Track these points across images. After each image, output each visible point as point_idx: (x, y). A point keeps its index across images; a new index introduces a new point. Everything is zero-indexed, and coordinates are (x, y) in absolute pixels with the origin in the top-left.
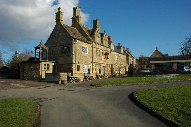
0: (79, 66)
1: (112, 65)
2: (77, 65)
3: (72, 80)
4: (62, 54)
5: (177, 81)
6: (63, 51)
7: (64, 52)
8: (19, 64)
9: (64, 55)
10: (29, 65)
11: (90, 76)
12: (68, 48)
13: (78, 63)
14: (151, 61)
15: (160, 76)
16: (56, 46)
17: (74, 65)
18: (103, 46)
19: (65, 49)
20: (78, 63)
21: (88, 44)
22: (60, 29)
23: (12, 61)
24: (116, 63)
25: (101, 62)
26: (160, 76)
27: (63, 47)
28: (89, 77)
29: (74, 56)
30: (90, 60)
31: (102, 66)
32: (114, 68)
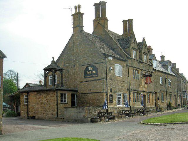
0: (111, 96)
4: (85, 78)
5: (160, 124)
6: (88, 73)
7: (88, 75)
9: (88, 79)
10: (36, 95)
16: (74, 66)
17: (105, 94)
19: (91, 70)
20: (111, 91)
29: (106, 80)
31: (142, 96)
32: (158, 99)
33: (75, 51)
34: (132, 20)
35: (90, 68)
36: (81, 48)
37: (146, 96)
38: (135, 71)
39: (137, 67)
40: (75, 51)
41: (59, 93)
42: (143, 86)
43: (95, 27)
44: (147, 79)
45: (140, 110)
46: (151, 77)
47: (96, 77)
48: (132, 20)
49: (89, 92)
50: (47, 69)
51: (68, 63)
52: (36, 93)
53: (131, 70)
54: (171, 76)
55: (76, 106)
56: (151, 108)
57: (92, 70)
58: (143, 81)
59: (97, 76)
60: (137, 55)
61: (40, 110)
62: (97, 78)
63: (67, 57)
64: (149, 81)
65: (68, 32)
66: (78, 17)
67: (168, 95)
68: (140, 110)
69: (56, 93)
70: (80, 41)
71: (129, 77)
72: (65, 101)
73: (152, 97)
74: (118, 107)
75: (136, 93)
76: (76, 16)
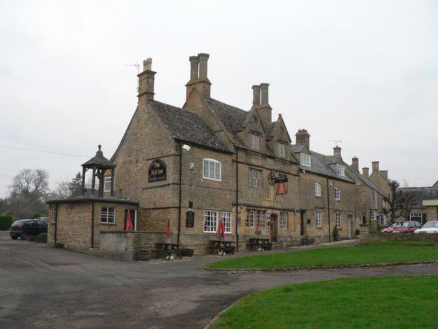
1: (302, 212)
3: (259, 245)
6: (153, 173)
8: (81, 177)
10: (67, 208)
11: (262, 240)
13: (191, 205)
14: (427, 198)
18: (272, 158)
19: (157, 168)
20: (191, 205)
21: (222, 155)
23: (25, 192)
24: (316, 205)
25: (266, 204)
28: (222, 245)
30: (228, 196)
32: (309, 221)
34: (268, 85)
36: (147, 130)
37: (279, 218)
39: (260, 164)
41: (98, 208)
42: (270, 199)
43: (189, 96)
44: (279, 186)
48: (268, 85)
49: (152, 206)
50: (88, 165)
51: (130, 156)
53: (243, 169)
54: (340, 183)
55: (135, 230)
56: (290, 237)
58: (272, 190)
59: (165, 179)
61: (70, 233)
65: (129, 104)
66: (147, 77)
67: (333, 216)
69: (91, 207)
71: (237, 181)
72: (111, 220)
73: (294, 219)
74: (207, 236)
75: (255, 210)
76: (143, 77)
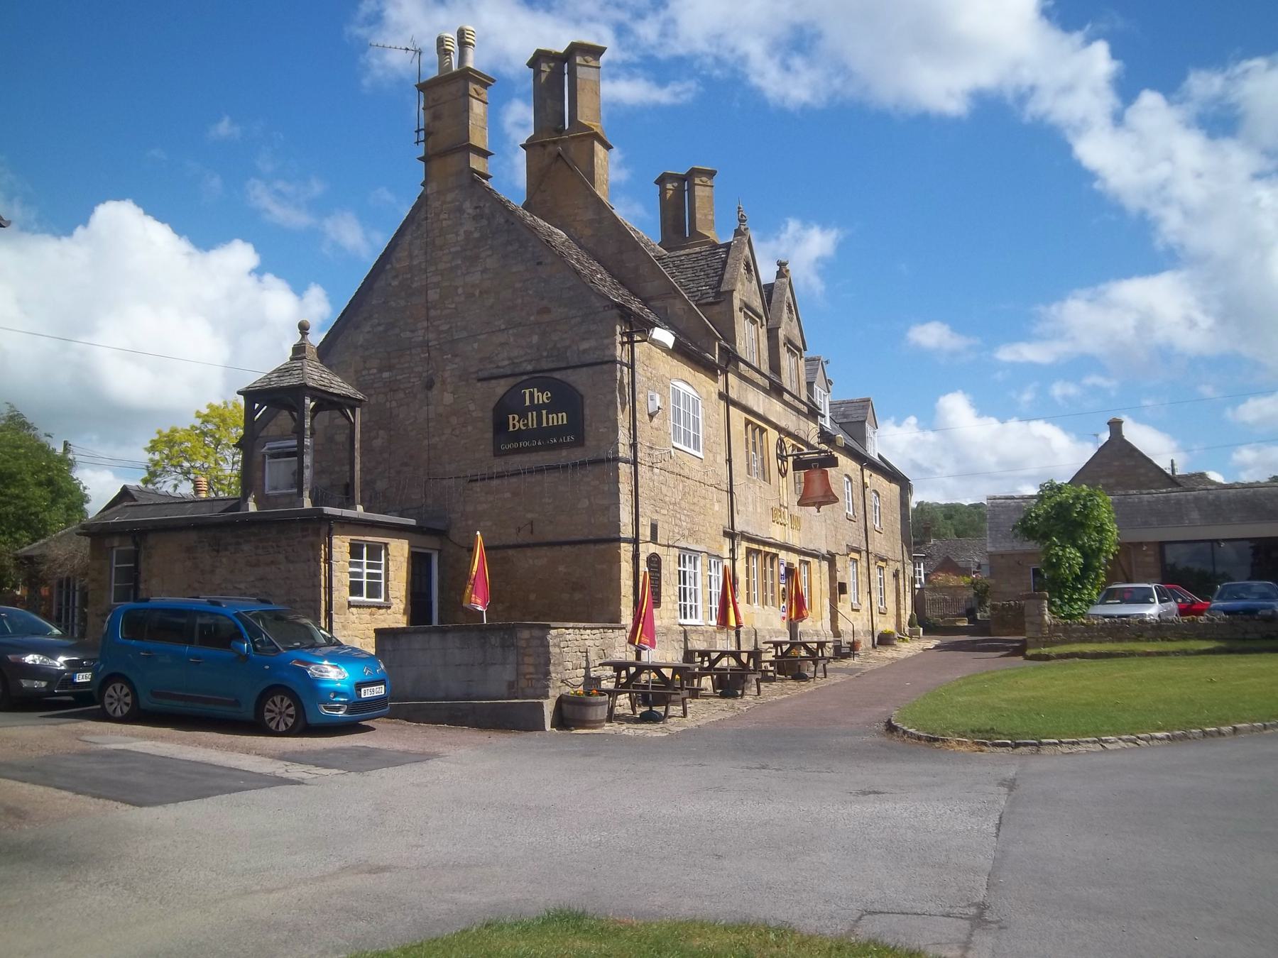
0: (654, 561)
2: (646, 550)
4: (498, 453)
6: (515, 423)
7: (518, 436)
9: (518, 461)
12: (566, 399)
15: (903, 551)
16: (429, 385)
17: (626, 550)
19: (538, 408)
22: (468, 225)
26: (903, 551)
27: (515, 392)
33: (433, 295)
35: (532, 395)
36: (476, 278)
38: (754, 431)
40: (433, 295)
45: (719, 659)
46: (831, 472)
47: (569, 445)
49: (524, 537)
51: (390, 368)
52: (193, 536)
57: (544, 406)
59: (580, 441)
60: (761, 346)
62: (577, 455)
63: (381, 328)
64: (817, 488)
68: (713, 663)
70: (468, 234)
